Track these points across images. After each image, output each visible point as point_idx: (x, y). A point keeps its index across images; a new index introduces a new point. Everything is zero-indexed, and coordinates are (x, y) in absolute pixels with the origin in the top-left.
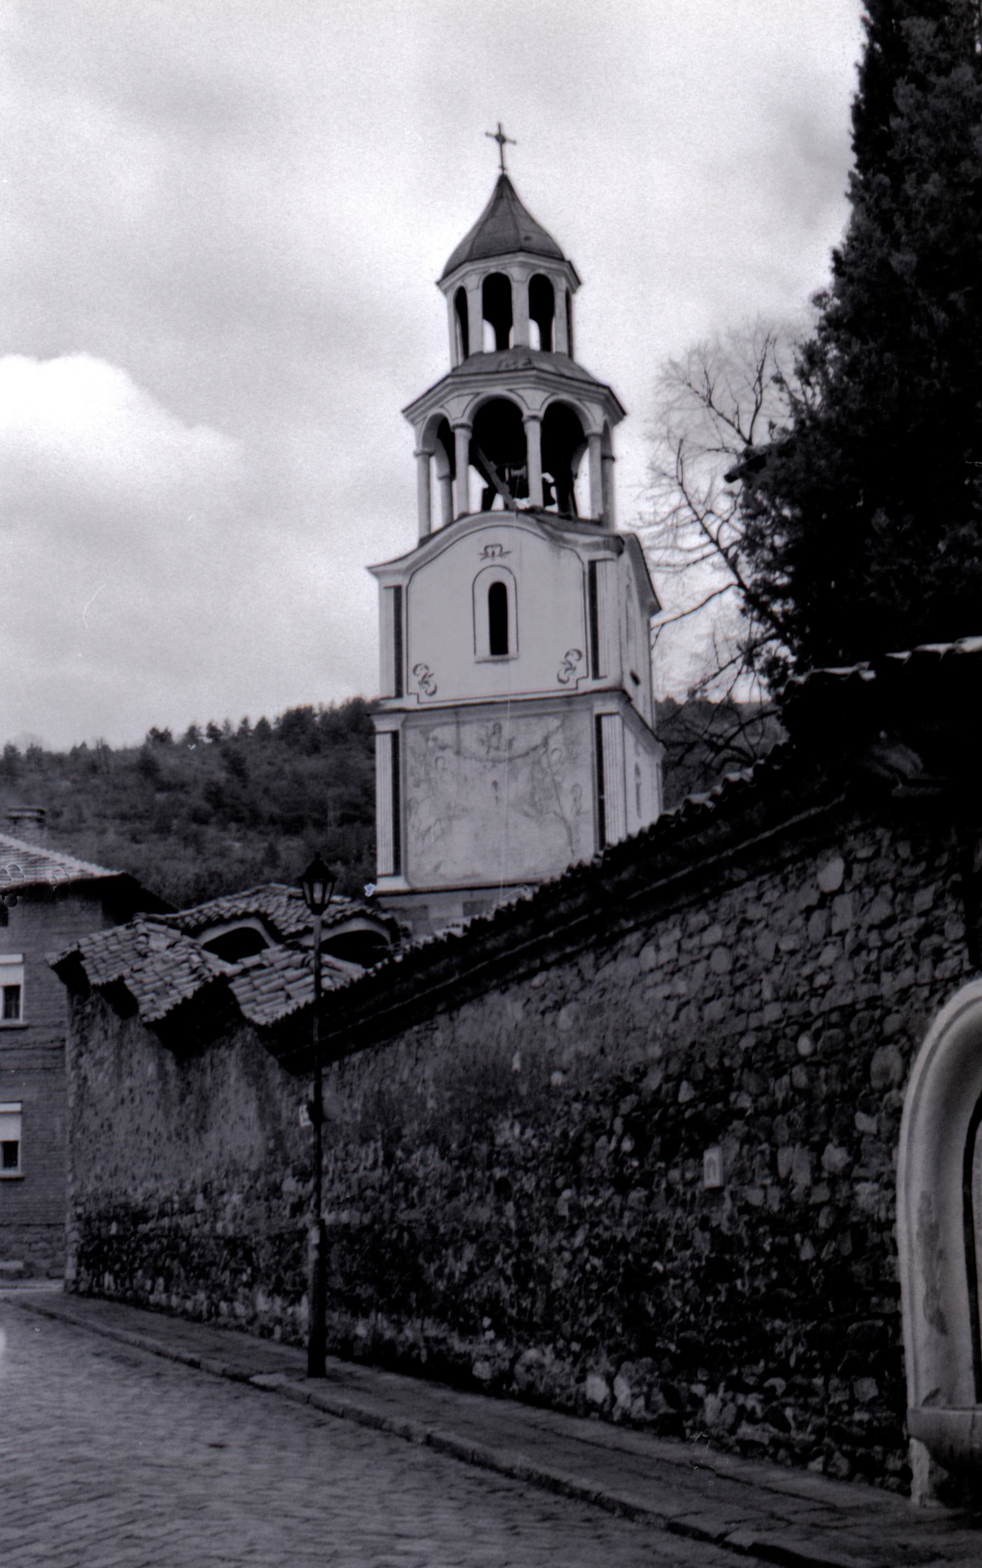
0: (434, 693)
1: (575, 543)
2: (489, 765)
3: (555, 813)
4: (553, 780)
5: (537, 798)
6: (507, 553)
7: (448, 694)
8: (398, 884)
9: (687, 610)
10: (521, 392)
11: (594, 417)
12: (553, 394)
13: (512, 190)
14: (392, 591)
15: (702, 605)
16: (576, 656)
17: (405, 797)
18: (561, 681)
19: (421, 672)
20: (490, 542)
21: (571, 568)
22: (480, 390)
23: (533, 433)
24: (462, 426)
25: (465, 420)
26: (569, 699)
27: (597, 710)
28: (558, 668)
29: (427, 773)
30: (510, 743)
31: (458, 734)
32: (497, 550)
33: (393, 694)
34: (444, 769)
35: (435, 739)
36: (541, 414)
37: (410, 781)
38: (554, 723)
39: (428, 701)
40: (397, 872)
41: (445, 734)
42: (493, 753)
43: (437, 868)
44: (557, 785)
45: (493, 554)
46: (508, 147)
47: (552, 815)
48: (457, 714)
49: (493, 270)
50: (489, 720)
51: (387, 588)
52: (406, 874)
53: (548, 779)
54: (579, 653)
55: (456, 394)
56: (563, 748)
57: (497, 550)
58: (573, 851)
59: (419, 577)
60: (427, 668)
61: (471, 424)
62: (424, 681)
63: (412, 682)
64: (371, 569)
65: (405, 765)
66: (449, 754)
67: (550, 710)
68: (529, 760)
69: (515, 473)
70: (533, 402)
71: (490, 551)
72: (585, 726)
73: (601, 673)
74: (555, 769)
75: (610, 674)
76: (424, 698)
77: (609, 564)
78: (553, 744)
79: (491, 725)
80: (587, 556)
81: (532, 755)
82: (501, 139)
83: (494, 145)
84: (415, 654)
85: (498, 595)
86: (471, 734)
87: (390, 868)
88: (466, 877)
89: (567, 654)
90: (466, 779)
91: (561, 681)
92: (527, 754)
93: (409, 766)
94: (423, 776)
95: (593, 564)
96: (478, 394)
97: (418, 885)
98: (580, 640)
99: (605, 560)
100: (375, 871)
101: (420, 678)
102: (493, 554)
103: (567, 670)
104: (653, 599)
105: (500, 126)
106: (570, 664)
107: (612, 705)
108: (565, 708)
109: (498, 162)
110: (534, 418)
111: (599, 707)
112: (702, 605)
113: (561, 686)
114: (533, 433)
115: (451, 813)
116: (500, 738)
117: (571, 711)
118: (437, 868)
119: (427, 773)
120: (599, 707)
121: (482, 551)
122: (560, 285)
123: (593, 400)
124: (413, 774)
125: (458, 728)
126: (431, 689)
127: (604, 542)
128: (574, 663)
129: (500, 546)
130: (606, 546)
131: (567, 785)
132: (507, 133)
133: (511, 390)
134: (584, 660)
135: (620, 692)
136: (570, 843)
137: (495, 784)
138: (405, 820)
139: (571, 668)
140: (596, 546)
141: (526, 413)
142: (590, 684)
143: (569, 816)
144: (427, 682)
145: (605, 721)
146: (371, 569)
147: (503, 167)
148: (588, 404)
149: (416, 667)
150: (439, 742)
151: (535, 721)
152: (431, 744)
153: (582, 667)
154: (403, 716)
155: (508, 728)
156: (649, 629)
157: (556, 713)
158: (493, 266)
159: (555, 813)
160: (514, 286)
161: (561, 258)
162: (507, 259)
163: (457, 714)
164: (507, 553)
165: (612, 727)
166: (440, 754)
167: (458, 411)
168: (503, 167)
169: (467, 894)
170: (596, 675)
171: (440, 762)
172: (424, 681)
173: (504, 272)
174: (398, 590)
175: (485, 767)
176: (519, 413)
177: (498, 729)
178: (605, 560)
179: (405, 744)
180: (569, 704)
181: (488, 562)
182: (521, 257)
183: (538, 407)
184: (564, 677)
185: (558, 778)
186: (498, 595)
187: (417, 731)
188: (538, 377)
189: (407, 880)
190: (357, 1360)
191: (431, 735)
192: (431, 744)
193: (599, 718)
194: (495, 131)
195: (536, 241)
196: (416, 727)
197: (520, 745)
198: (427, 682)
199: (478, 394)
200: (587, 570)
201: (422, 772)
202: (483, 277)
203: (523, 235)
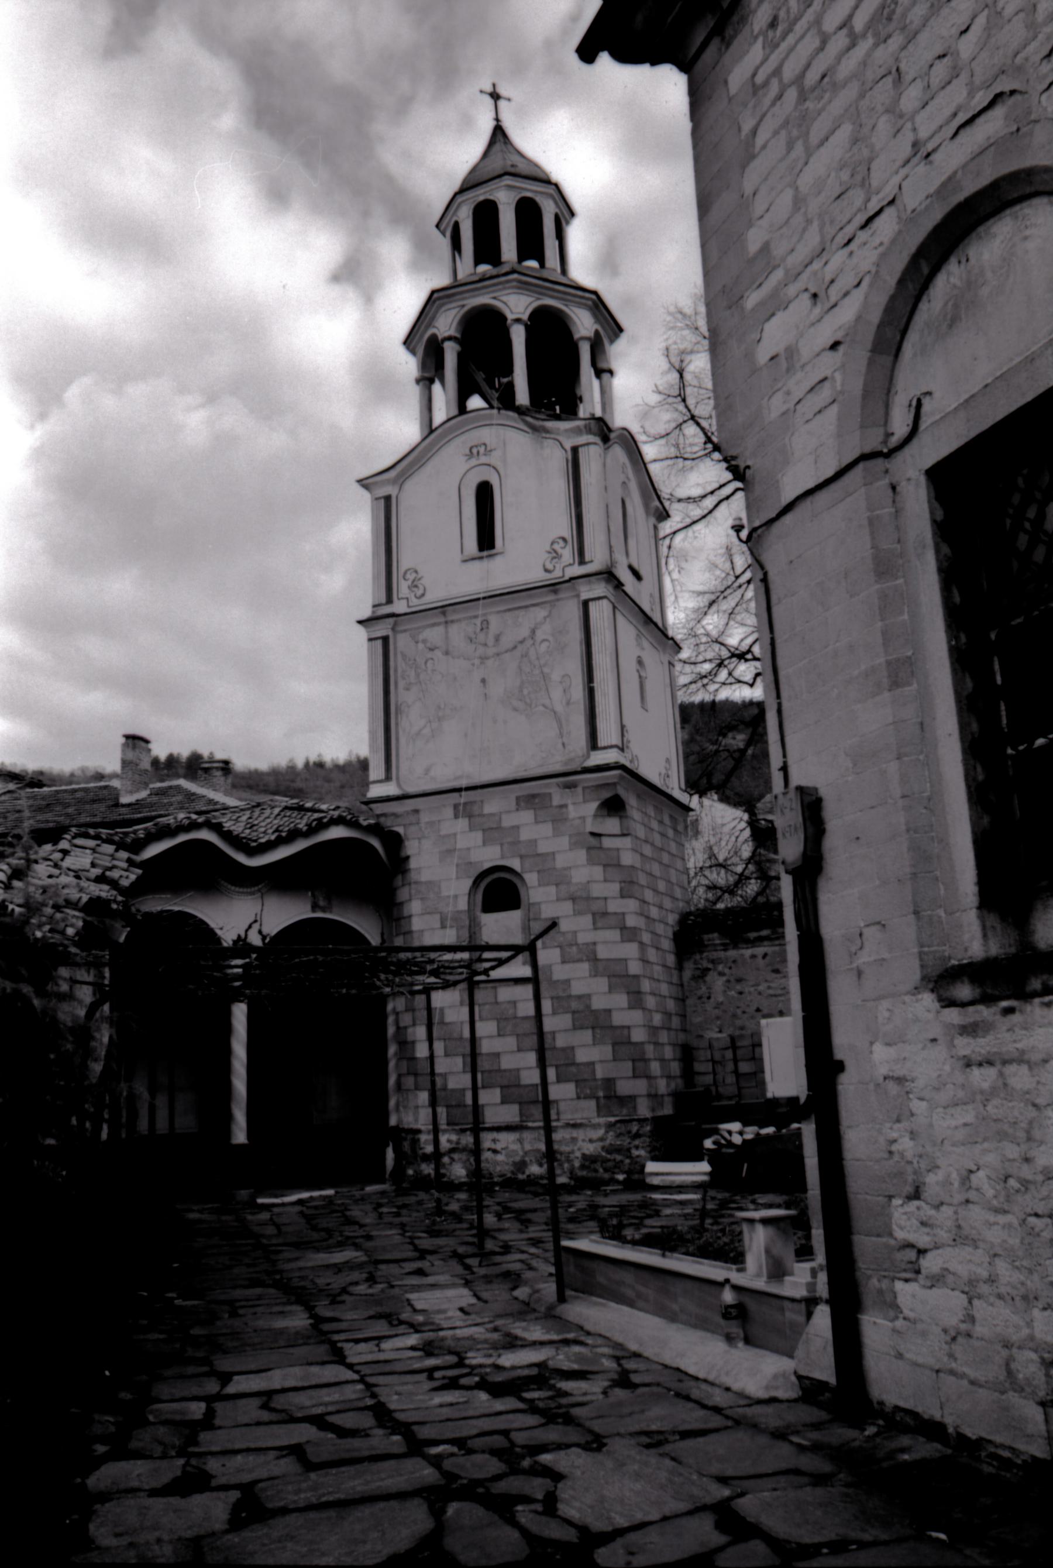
0: (423, 595)
1: (558, 432)
2: (477, 662)
3: (544, 706)
4: (542, 672)
5: (525, 692)
6: (491, 451)
7: (436, 595)
8: (390, 789)
9: (696, 519)
10: (504, 299)
11: (584, 324)
12: (538, 299)
13: (505, 135)
14: (382, 501)
15: (710, 512)
16: (562, 543)
17: (397, 702)
18: (546, 570)
19: (411, 576)
20: (475, 443)
21: (556, 459)
22: (465, 302)
23: (518, 337)
24: (449, 338)
25: (452, 332)
26: (553, 587)
27: (584, 596)
28: (544, 557)
29: (418, 675)
30: (497, 639)
31: (447, 632)
32: (482, 449)
33: (384, 601)
34: (433, 671)
35: (424, 641)
36: (525, 317)
37: (402, 684)
38: (540, 613)
39: (417, 604)
40: (388, 778)
41: (434, 634)
42: (481, 650)
43: (427, 771)
44: (545, 677)
45: (478, 453)
46: (502, 104)
47: (541, 708)
48: (444, 614)
49: (481, 198)
50: (476, 617)
51: (377, 499)
52: (398, 779)
53: (537, 672)
54: (564, 539)
55: (443, 309)
56: (551, 638)
57: (482, 449)
58: (563, 744)
59: (409, 485)
60: (416, 572)
61: (458, 335)
62: (414, 586)
63: (402, 588)
64: (359, 481)
65: (396, 671)
66: (438, 653)
67: (534, 602)
68: (517, 653)
69: (505, 380)
70: (517, 305)
71: (475, 451)
72: (571, 611)
73: (587, 558)
74: (542, 662)
75: (597, 560)
76: (414, 601)
77: (592, 448)
78: (540, 635)
79: (478, 622)
80: (568, 445)
81: (520, 647)
82: (495, 96)
83: (489, 101)
84: (406, 558)
85: (485, 494)
86: (458, 633)
87: (382, 775)
88: (456, 778)
89: (552, 543)
90: (455, 679)
91: (546, 570)
92: (515, 647)
93: (400, 671)
94: (413, 679)
95: (575, 450)
96: (463, 306)
97: (411, 790)
98: (564, 526)
99: (588, 444)
100: (367, 776)
101: (410, 582)
102: (478, 453)
103: (553, 558)
104: (657, 503)
105: (494, 85)
106: (555, 552)
107: (600, 589)
108: (551, 597)
109: (493, 115)
110: (518, 321)
111: (586, 592)
112: (710, 512)
113: (548, 576)
114: (518, 337)
115: (440, 714)
116: (487, 634)
117: (558, 600)
118: (427, 771)
119: (418, 675)
120: (586, 592)
121: (467, 451)
122: (549, 210)
123: (580, 305)
124: (404, 678)
125: (446, 627)
126: (419, 592)
127: (585, 426)
128: (560, 551)
129: (485, 444)
130: (589, 431)
131: (556, 676)
132: (502, 91)
133: (494, 298)
134: (569, 547)
135: (609, 575)
136: (561, 735)
137: (483, 681)
138: (397, 724)
139: (556, 556)
140: (578, 431)
141: (510, 316)
142: (577, 570)
143: (559, 708)
144: (416, 586)
145: (592, 606)
146: (359, 481)
147: (497, 120)
148: (574, 309)
149: (405, 573)
150: (429, 645)
151: (522, 612)
152: (421, 646)
153: (567, 554)
154: (391, 620)
155: (494, 621)
156: (657, 539)
157: (543, 603)
158: (480, 195)
159: (544, 706)
160: (501, 208)
161: (547, 181)
162: (492, 185)
163: (444, 614)
164: (491, 451)
165: (600, 612)
166: (430, 655)
167: (446, 324)
168: (497, 120)
169: (456, 795)
170: (582, 562)
171: (430, 663)
172: (414, 586)
173: (491, 198)
174: (388, 499)
175: (473, 665)
176: (504, 318)
177: (485, 626)
178: (588, 444)
179: (395, 648)
180: (555, 592)
181: (474, 462)
182: (508, 181)
183: (521, 310)
184: (550, 566)
185: (546, 670)
186: (485, 494)
187: (407, 634)
188: (520, 281)
189: (399, 785)
190: (666, 1241)
191: (421, 637)
192: (421, 646)
193: (586, 604)
194: (489, 89)
195: (522, 168)
196: (405, 631)
197: (507, 641)
198: (416, 586)
199: (463, 306)
200: (570, 458)
201: (413, 673)
202: (472, 207)
203: (509, 163)
